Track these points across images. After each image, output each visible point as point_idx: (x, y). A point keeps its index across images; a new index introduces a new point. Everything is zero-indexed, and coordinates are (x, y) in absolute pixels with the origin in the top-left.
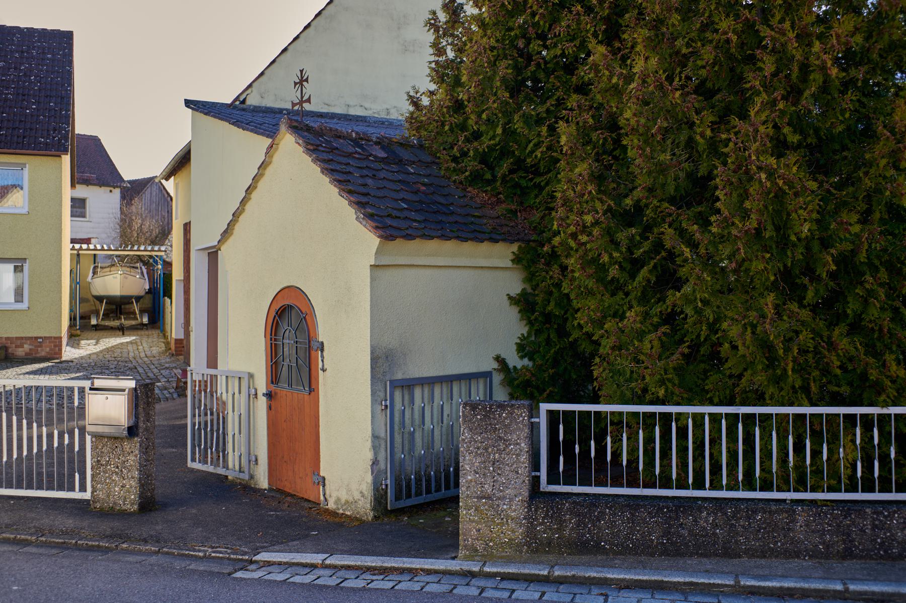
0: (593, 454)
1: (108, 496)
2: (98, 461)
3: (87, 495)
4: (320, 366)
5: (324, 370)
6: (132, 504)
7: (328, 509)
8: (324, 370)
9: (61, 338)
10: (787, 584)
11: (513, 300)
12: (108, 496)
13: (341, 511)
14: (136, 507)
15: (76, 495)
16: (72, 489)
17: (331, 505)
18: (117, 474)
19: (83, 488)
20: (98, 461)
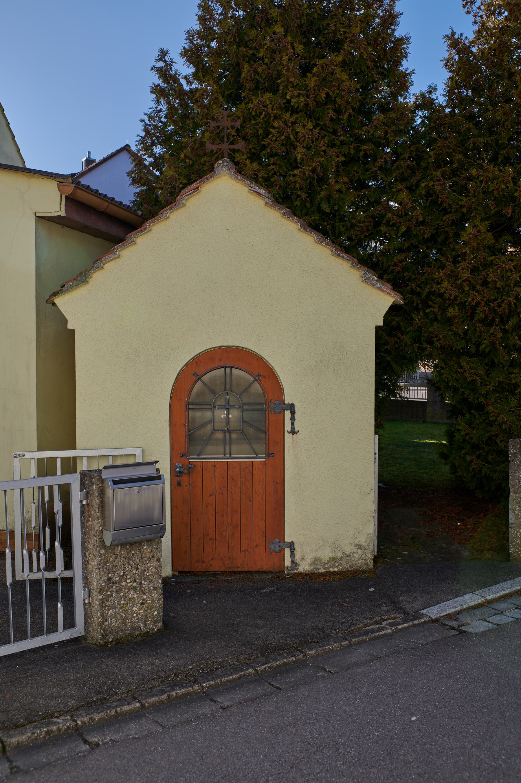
0: (436, 442)
1: (124, 622)
2: (109, 579)
3: (79, 630)
4: (288, 427)
5: (293, 432)
6: (155, 622)
7: (300, 574)
8: (293, 432)
9: (74, 448)
10: (505, 592)
11: (129, 174)
12: (124, 622)
13: (322, 570)
14: (160, 624)
15: (62, 635)
16: (53, 628)
17: (304, 567)
18: (135, 589)
19: (70, 623)
20: (109, 579)
